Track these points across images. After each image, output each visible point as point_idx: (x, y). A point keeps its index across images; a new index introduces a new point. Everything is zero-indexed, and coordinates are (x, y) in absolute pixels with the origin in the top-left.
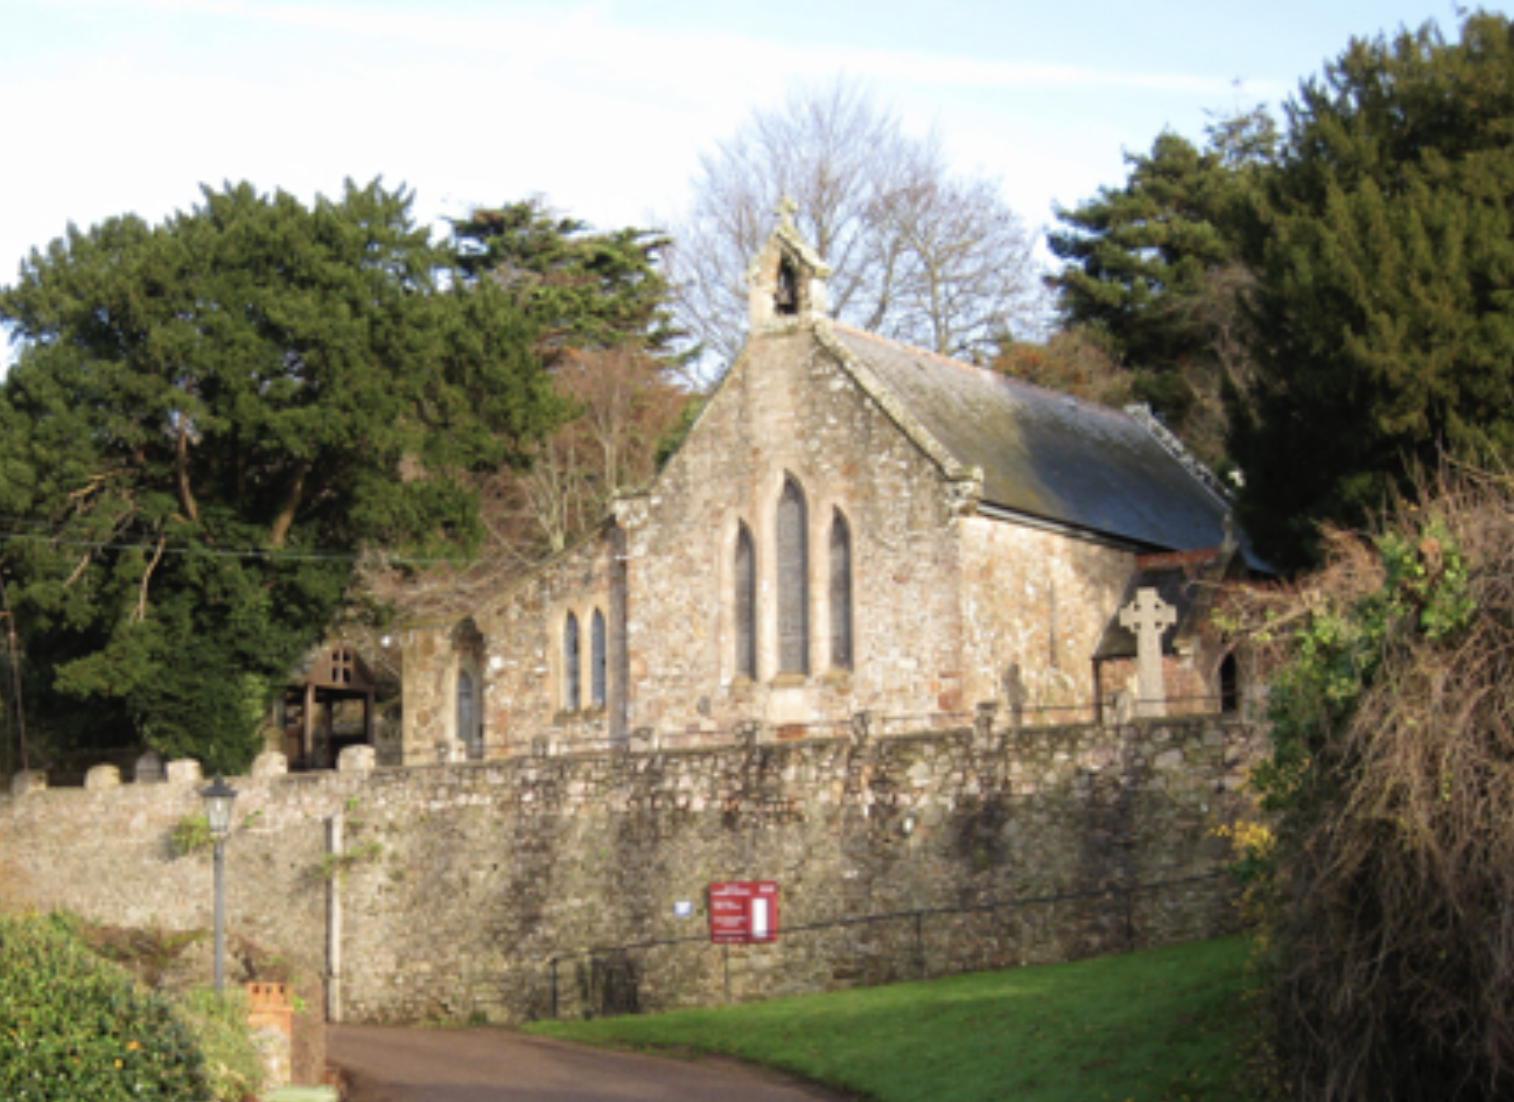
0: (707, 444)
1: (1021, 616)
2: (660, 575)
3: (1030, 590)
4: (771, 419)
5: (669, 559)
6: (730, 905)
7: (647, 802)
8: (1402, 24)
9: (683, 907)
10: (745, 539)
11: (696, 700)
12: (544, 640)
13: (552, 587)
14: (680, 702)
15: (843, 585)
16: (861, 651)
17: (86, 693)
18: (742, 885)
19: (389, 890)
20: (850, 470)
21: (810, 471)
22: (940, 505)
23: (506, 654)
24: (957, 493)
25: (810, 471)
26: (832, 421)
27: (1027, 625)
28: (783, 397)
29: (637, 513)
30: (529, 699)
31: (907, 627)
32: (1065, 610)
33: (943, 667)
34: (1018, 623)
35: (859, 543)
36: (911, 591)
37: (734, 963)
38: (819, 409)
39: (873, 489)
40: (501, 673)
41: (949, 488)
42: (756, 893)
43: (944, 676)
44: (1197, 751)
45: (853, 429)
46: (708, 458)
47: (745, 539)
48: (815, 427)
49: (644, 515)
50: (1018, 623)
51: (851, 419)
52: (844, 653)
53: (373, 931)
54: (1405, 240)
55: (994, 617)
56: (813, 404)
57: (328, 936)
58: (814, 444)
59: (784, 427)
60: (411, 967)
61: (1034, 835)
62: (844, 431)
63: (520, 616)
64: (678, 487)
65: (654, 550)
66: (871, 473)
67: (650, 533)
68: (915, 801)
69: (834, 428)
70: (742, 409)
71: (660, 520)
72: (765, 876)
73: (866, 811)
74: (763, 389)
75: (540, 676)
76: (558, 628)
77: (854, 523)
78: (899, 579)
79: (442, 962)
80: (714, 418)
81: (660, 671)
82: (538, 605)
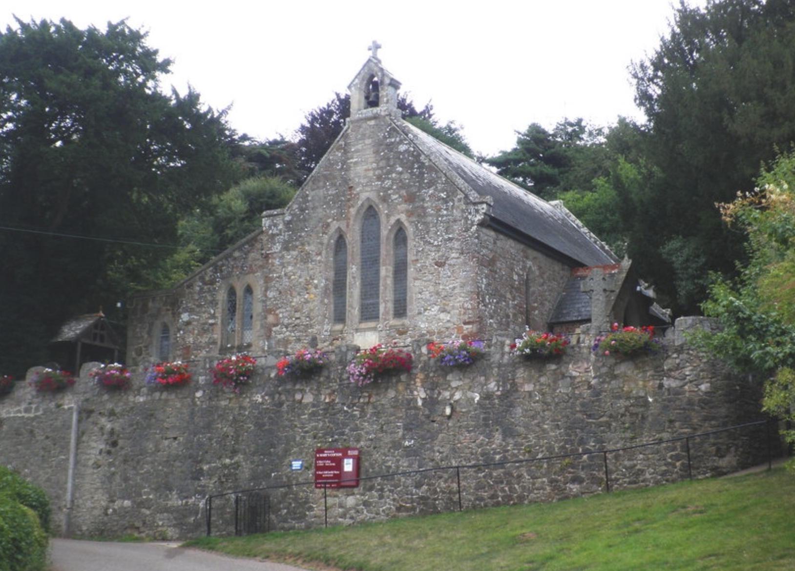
0: (321, 184)
1: (511, 293)
2: (289, 263)
3: (515, 277)
4: (360, 169)
5: (295, 253)
6: (328, 463)
7: (277, 396)
8: (619, 116)
9: (296, 465)
10: (340, 243)
11: (309, 338)
12: (214, 303)
13: (221, 271)
14: (299, 340)
15: (400, 270)
16: (413, 307)
17: (103, 30)
18: (337, 451)
19: (109, 453)
20: (410, 199)
21: (385, 199)
22: (467, 219)
23: (191, 311)
24: (477, 211)
25: (385, 199)
26: (400, 169)
27: (514, 299)
28: (369, 155)
29: (276, 225)
30: (204, 339)
31: (444, 294)
32: (534, 293)
33: (466, 318)
34: (509, 296)
35: (412, 243)
36: (445, 271)
37: (330, 501)
38: (392, 163)
39: (424, 209)
40: (188, 323)
41: (472, 208)
42: (346, 456)
43: (465, 323)
44: (605, 396)
45: (412, 174)
46: (321, 192)
47: (340, 243)
48: (389, 172)
49: (281, 227)
50: (509, 296)
51: (412, 168)
52: (400, 310)
53: (92, 479)
54: (355, 539)
55: (496, 290)
56: (388, 159)
57: (76, 455)
58: (388, 183)
59: (371, 174)
60: (118, 504)
61: (533, 417)
62: (406, 176)
63: (202, 289)
64: (302, 210)
65: (286, 248)
66: (423, 200)
67: (285, 236)
68: (452, 396)
69: (401, 173)
70: (344, 163)
71: (289, 229)
72: (352, 444)
73: (420, 403)
74: (357, 151)
75: (212, 325)
76: (222, 296)
77: (410, 230)
78: (440, 264)
79: (139, 500)
80: (326, 168)
81: (286, 321)
82: (212, 282)
